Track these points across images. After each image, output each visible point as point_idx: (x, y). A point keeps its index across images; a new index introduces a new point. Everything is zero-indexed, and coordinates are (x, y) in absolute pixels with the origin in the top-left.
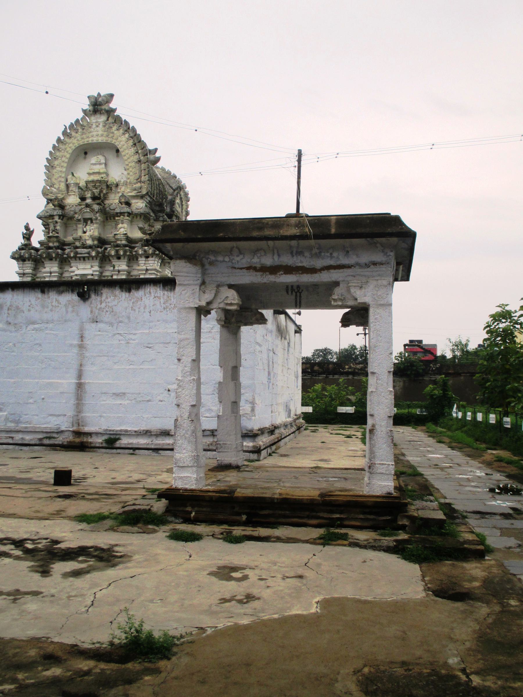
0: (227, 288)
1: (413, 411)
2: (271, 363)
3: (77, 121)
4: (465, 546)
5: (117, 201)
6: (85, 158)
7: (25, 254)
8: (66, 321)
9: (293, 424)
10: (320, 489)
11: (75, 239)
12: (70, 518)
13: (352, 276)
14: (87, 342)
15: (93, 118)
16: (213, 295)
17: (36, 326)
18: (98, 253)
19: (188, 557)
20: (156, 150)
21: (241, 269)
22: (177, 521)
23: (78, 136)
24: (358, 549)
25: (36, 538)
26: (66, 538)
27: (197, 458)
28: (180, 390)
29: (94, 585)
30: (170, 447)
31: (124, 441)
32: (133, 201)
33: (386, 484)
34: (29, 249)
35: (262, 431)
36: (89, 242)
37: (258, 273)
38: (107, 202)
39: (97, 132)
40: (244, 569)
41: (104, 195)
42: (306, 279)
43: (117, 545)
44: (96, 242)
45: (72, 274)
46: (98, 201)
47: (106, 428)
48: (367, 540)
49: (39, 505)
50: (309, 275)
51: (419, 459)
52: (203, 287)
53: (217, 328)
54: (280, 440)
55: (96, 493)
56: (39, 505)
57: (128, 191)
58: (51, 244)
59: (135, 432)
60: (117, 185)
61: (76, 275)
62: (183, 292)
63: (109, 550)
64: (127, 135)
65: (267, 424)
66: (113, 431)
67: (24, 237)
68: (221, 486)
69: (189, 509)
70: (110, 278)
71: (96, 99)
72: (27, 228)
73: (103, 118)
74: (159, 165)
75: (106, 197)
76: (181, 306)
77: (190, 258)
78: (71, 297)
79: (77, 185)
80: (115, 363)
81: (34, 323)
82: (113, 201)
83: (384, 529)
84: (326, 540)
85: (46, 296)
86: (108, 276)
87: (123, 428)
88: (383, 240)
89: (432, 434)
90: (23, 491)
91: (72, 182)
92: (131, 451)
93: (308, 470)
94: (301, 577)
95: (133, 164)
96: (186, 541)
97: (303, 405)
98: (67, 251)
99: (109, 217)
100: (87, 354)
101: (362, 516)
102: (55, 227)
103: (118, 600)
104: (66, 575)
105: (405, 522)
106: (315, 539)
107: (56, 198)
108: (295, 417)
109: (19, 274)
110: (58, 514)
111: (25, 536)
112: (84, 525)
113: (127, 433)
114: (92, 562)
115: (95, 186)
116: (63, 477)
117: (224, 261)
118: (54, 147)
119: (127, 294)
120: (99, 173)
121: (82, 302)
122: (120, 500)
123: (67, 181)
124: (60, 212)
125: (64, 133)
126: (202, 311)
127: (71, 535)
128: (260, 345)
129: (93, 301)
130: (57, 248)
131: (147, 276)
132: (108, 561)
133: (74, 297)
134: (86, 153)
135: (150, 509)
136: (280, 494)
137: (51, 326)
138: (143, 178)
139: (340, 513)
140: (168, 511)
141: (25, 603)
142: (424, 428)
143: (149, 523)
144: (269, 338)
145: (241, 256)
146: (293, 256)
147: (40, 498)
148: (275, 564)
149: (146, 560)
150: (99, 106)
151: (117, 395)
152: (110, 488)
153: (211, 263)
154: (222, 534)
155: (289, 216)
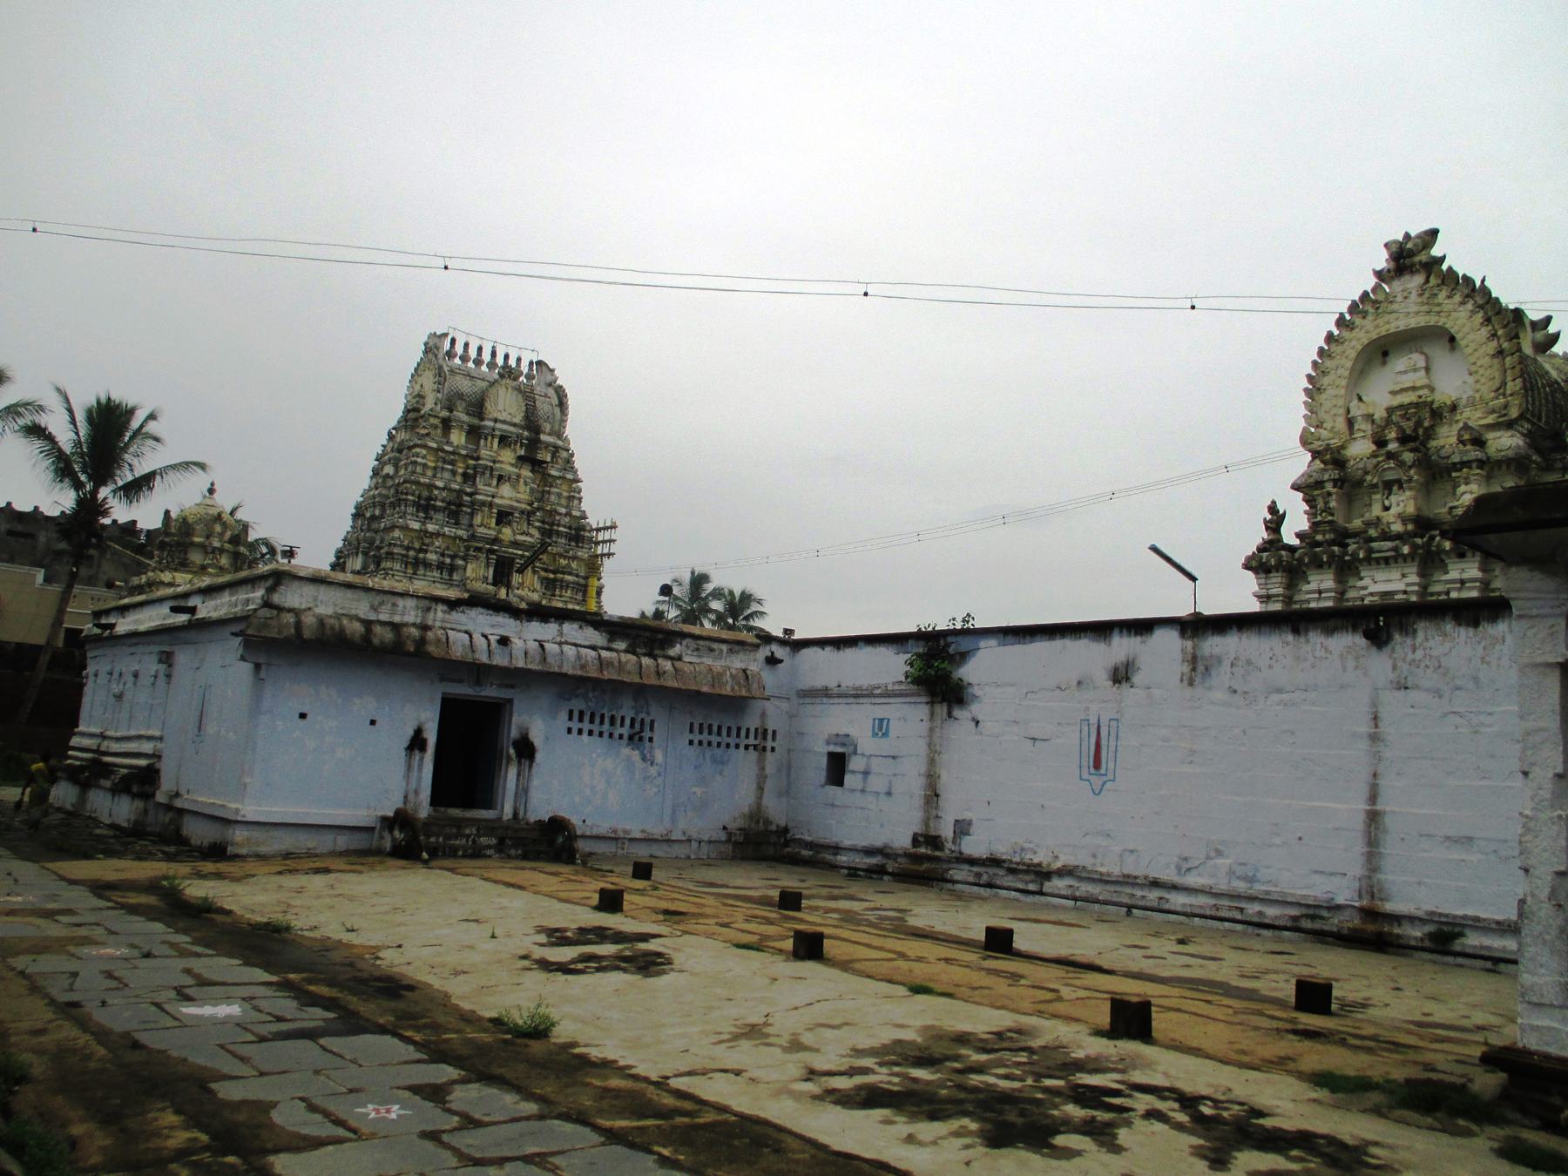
3: (1365, 295)
5: (1454, 440)
6: (1384, 363)
7: (1270, 559)
11: (1368, 524)
12: (1300, 1075)
14: (1384, 727)
15: (1396, 283)
17: (1285, 696)
18: (1414, 547)
20: (1548, 320)
22: (1526, 1122)
23: (1368, 323)
25: (1222, 1098)
26: (1279, 1111)
28: (1528, 837)
30: (1512, 957)
31: (1473, 940)
32: (1490, 436)
34: (1278, 549)
36: (1397, 527)
38: (1433, 444)
39: (1408, 312)
41: (1426, 429)
43: (1376, 1144)
44: (1410, 527)
45: (1362, 592)
46: (1412, 445)
49: (1247, 1040)
56: (1247, 1040)
57: (1476, 418)
58: (1319, 537)
59: (1498, 923)
61: (1372, 594)
62: (1530, 633)
63: (1356, 1149)
64: (1470, 306)
66: (1447, 916)
67: (1267, 528)
70: (1443, 597)
71: (1401, 245)
72: (1273, 509)
73: (1418, 279)
74: (1558, 349)
75: (1430, 433)
77: (1539, 561)
78: (1348, 642)
79: (1369, 417)
81: (1279, 691)
82: (1446, 438)
85: (1302, 639)
86: (1439, 594)
87: (1470, 912)
90: (1230, 1011)
91: (1359, 413)
92: (1489, 965)
95: (1487, 360)
96: (1536, 1168)
98: (1351, 548)
99: (1437, 473)
102: (1326, 503)
110: (1280, 1064)
111: (1205, 1091)
112: (1322, 1094)
113: (1479, 925)
115: (1406, 417)
116: (1313, 996)
118: (1321, 352)
119: (1471, 631)
120: (1414, 388)
121: (1374, 649)
123: (1348, 412)
124: (1335, 474)
125: (1341, 322)
127: (1291, 1105)
129: (1398, 648)
130: (1333, 543)
131: (1466, 594)
133: (1359, 640)
134: (1385, 354)
135: (1464, 1086)
138: (1510, 385)
140: (1505, 1095)
147: (1256, 1028)
152: (1409, 1032)
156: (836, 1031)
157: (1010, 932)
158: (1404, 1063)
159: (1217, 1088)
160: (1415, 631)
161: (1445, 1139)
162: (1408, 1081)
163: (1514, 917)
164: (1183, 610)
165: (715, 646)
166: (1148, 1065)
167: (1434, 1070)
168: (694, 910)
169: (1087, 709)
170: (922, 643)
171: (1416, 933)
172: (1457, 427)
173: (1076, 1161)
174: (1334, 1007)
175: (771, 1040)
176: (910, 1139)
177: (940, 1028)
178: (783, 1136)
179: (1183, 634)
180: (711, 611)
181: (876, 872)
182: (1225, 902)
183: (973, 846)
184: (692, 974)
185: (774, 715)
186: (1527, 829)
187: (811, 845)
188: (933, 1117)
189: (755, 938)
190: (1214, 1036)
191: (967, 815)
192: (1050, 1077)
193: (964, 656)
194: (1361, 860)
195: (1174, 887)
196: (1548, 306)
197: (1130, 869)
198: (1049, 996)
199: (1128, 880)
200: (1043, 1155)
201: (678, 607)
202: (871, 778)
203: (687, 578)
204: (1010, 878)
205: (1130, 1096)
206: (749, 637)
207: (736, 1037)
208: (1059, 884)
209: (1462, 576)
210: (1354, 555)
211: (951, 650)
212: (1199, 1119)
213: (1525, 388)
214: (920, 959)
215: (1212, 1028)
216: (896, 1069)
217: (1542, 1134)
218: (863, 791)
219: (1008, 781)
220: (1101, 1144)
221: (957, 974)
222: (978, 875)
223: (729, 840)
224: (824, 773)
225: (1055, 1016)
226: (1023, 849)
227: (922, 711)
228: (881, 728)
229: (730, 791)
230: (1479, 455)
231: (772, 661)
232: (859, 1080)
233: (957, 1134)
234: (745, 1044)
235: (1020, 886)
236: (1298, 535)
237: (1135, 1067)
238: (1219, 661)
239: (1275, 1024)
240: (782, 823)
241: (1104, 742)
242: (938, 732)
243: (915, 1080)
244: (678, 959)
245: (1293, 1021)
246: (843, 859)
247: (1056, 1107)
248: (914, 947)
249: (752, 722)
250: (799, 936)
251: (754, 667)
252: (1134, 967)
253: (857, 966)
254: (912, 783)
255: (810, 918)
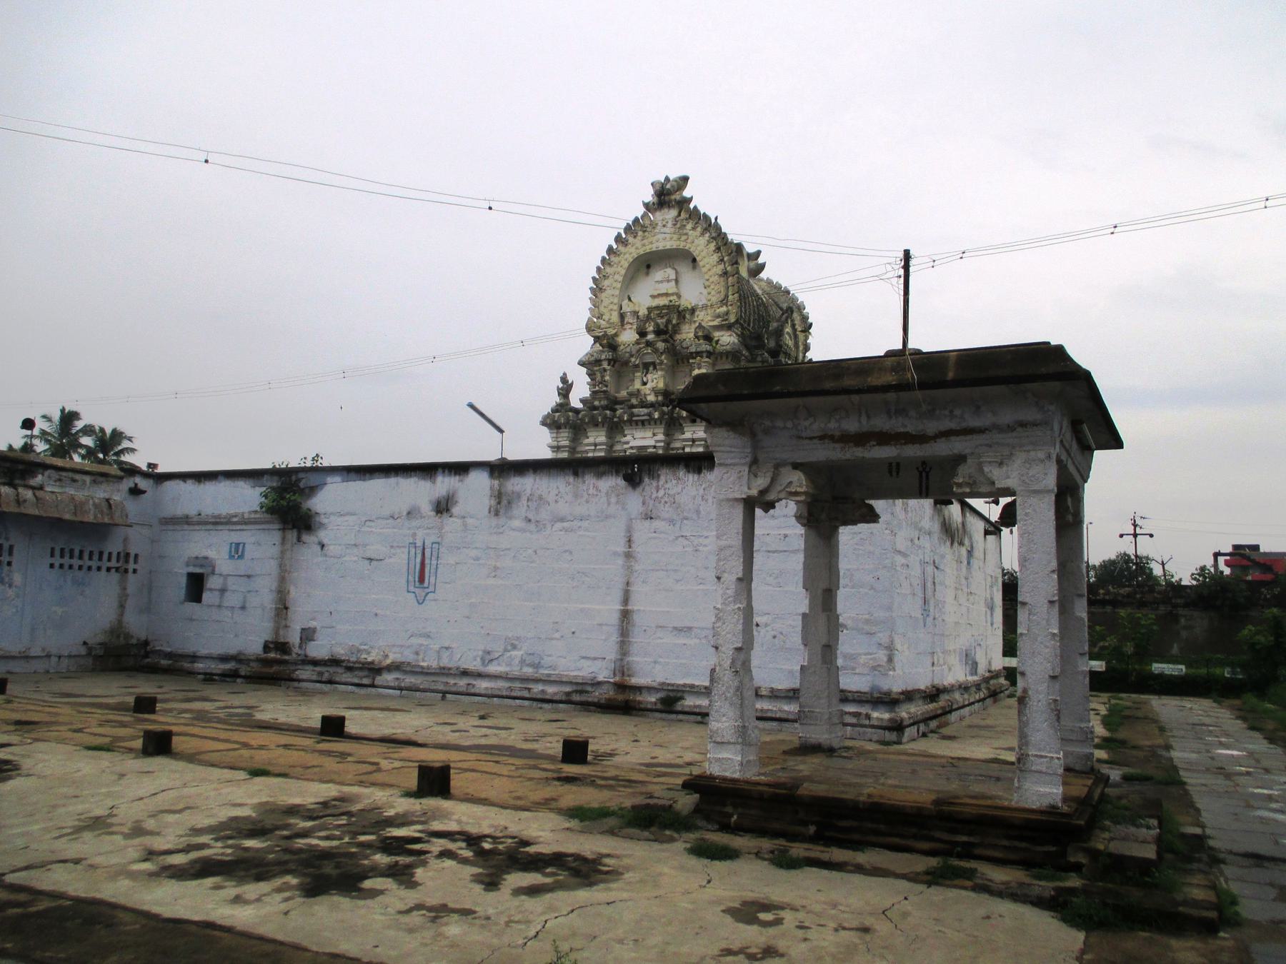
0: (790, 468)
1: (1218, 671)
2: (929, 585)
3: (636, 220)
4: (1181, 909)
5: (692, 335)
6: (647, 274)
7: (562, 419)
8: (607, 517)
9: (983, 686)
10: (938, 792)
11: (631, 395)
12: (560, 811)
13: (987, 445)
15: (658, 214)
16: (768, 480)
17: (565, 524)
18: (663, 414)
19: (704, 883)
20: (758, 253)
21: (811, 438)
23: (638, 242)
24: (987, 896)
27: (743, 731)
29: (551, 908)
31: (690, 702)
32: (717, 334)
33: (1048, 790)
35: (909, 696)
36: (651, 398)
37: (837, 445)
38: (678, 337)
39: (663, 240)
40: (782, 908)
41: (674, 326)
42: (913, 451)
43: (608, 856)
44: (660, 398)
46: (663, 337)
47: (663, 680)
48: (1006, 883)
50: (917, 446)
51: (1194, 756)
52: (754, 467)
53: (797, 532)
54: (950, 712)
55: (615, 778)
58: (596, 403)
60: (693, 311)
65: (923, 683)
68: (783, 777)
69: (729, 809)
72: (564, 379)
73: (674, 213)
74: (763, 275)
75: (676, 329)
76: (722, 497)
77: (734, 424)
79: (635, 313)
80: (677, 581)
81: (562, 520)
82: (687, 334)
83: (1041, 866)
84: (934, 878)
87: (688, 681)
88: (1036, 386)
89: (1244, 715)
92: (699, 718)
93: (943, 761)
94: (866, 930)
97: (1005, 654)
98: (618, 412)
100: (637, 567)
101: (1006, 843)
102: (603, 377)
103: (574, 934)
104: (518, 892)
105: (1082, 859)
106: (918, 874)
107: (605, 335)
108: (987, 674)
109: (552, 447)
111: (487, 831)
112: (574, 823)
114: (562, 876)
116: (575, 751)
117: (785, 428)
118: (603, 260)
119: (696, 477)
120: (667, 295)
122: (644, 789)
125: (618, 239)
126: (754, 504)
128: (905, 555)
130: (605, 408)
131: (694, 450)
132: (586, 876)
133: (620, 482)
134: (648, 267)
135: (671, 806)
136: (870, 796)
137: (585, 524)
138: (730, 297)
139: (970, 834)
140: (697, 810)
141: (446, 924)
142: (1237, 702)
143: (665, 826)
144: (926, 542)
145: (811, 420)
146: (890, 417)
147: (531, 779)
148: (834, 906)
149: (641, 881)
150: (669, 196)
151: (678, 630)
152: (641, 772)
153: (767, 432)
154: (772, 852)
155: (890, 354)
156: (177, 816)
157: (342, 719)
158: (633, 794)
159: (496, 827)
160: (659, 476)
161: (656, 846)
162: (634, 807)
163: (707, 684)
164: (492, 456)
165: (77, 477)
166: (445, 815)
167: (651, 797)
168: (47, 719)
169: (414, 535)
170: (276, 478)
171: (652, 698)
172: (694, 326)
173: (380, 898)
174: (589, 758)
175: (114, 829)
176: (238, 900)
177: (274, 803)
178: (121, 915)
179: (492, 475)
180: (81, 446)
181: (232, 675)
182: (518, 685)
183: (318, 649)
184: (39, 777)
185: (137, 541)
186: (718, 619)
187: (170, 655)
188: (259, 878)
189: (107, 740)
190: (497, 788)
191: (313, 624)
192: (364, 834)
193: (313, 490)
194: (616, 647)
195: (480, 675)
196: (759, 240)
197: (445, 662)
198: (370, 768)
199: (444, 672)
200: (353, 898)
201: (47, 441)
202: (227, 594)
203: (56, 416)
204: (349, 674)
205: (428, 842)
206: (114, 470)
207: (78, 830)
208: (388, 678)
209: (694, 436)
210: (620, 418)
211: (302, 485)
212: (482, 853)
213: (740, 300)
214: (261, 747)
215: (497, 782)
216: (230, 842)
217: (720, 834)
218: (219, 606)
219: (352, 595)
220: (401, 883)
221: (294, 757)
222: (321, 674)
223: (89, 654)
224: (183, 592)
225: (374, 784)
226: (359, 651)
227: (276, 536)
228: (237, 551)
229: (93, 608)
230: (709, 348)
231: (136, 492)
232: (194, 855)
233: (279, 890)
234: (87, 835)
235: (356, 681)
236: (582, 401)
237: (434, 818)
238: (519, 496)
239: (545, 774)
240: (143, 638)
241: (427, 561)
242: (288, 554)
243: (247, 849)
244: (26, 764)
245: (559, 771)
246: (200, 666)
247: (367, 857)
248: (257, 738)
249: (114, 546)
250: (148, 735)
251: (117, 497)
252: (441, 740)
253: (201, 757)
254: (264, 597)
255: (162, 719)
